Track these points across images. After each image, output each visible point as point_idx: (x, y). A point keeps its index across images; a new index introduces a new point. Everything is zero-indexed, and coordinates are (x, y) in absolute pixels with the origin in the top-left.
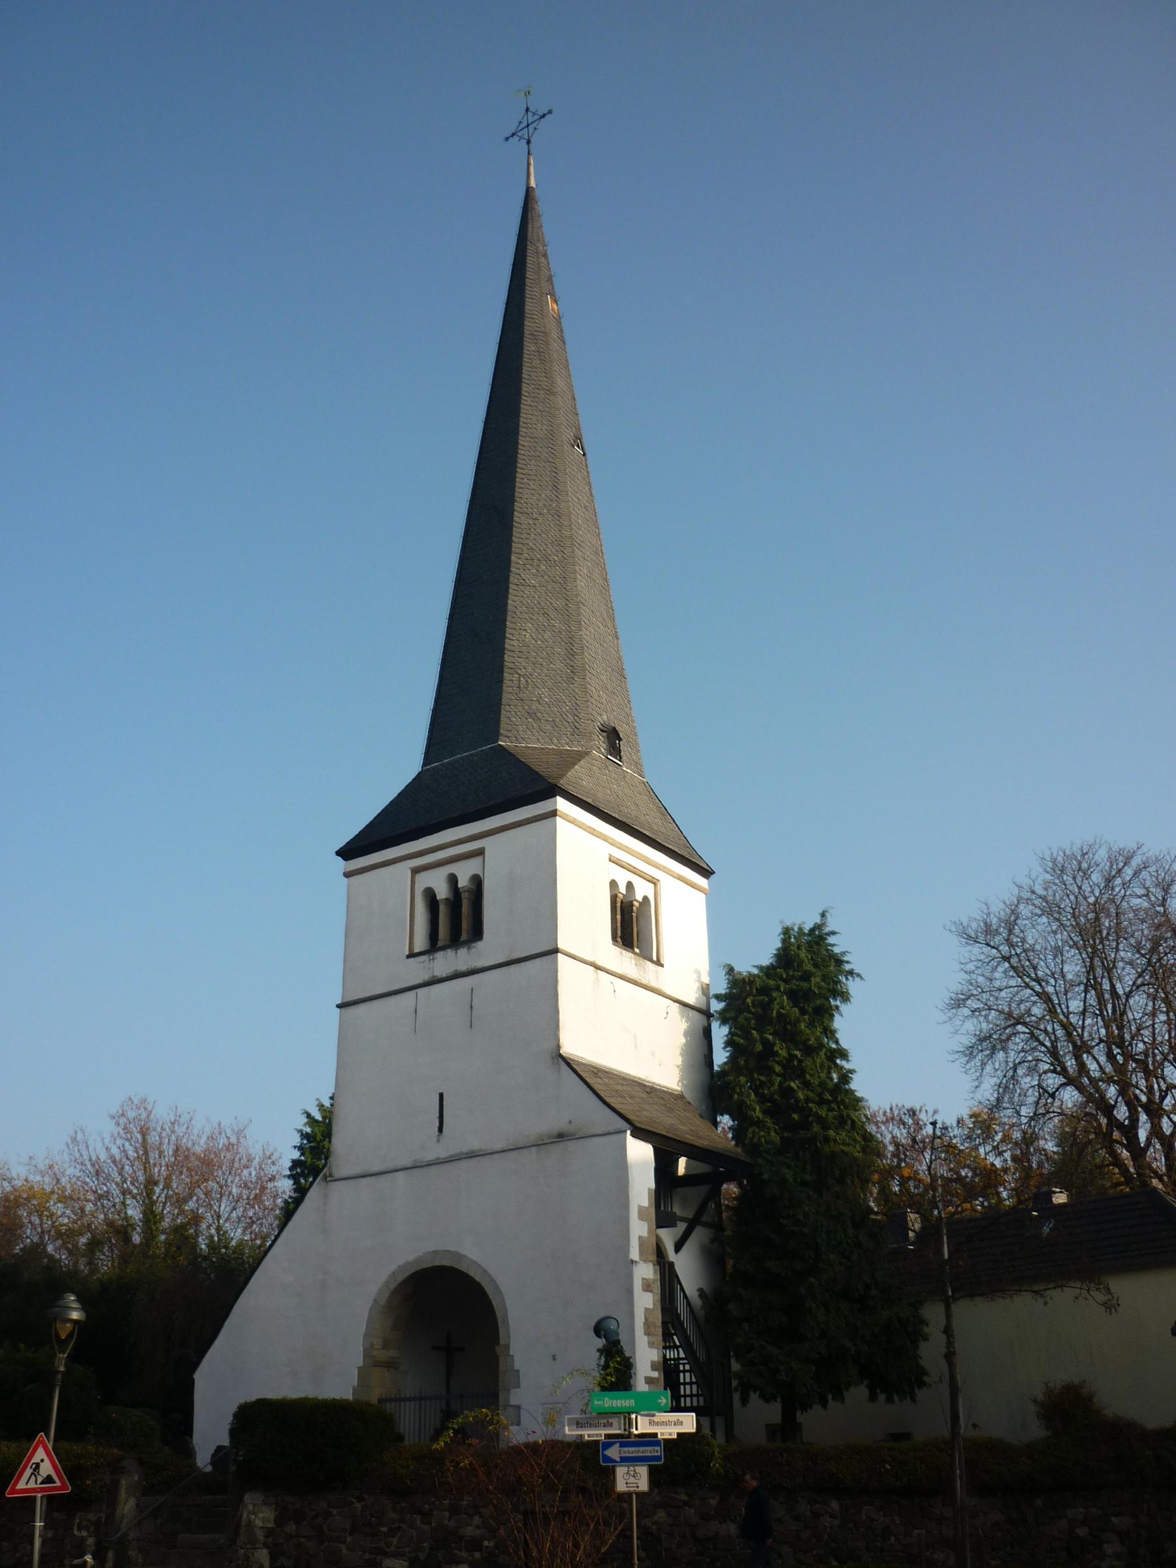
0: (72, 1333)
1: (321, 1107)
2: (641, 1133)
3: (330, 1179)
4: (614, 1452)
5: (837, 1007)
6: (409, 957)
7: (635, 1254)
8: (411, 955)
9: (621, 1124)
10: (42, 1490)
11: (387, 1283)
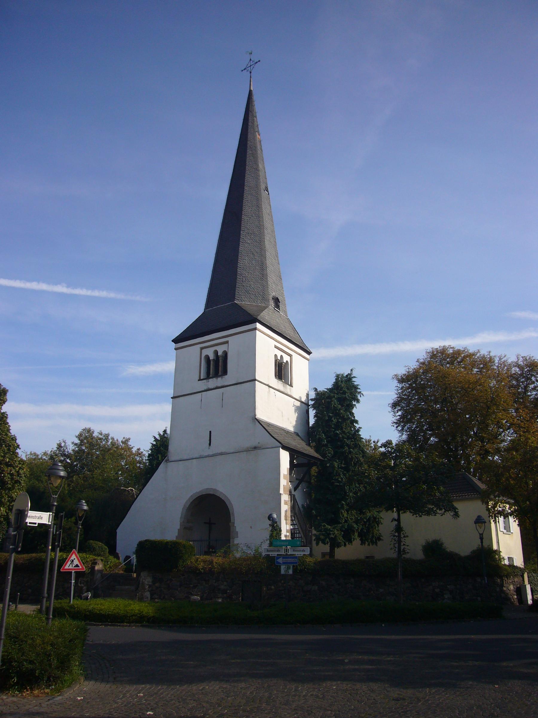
0: (83, 514)
1: (160, 435)
2: (285, 448)
3: (168, 461)
4: (280, 560)
5: (355, 405)
6: (199, 380)
7: (281, 491)
8: (200, 380)
9: (280, 445)
10: (74, 569)
11: (189, 499)
